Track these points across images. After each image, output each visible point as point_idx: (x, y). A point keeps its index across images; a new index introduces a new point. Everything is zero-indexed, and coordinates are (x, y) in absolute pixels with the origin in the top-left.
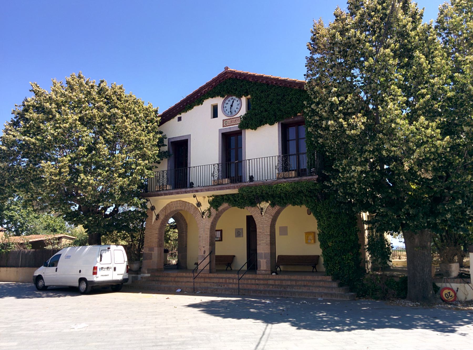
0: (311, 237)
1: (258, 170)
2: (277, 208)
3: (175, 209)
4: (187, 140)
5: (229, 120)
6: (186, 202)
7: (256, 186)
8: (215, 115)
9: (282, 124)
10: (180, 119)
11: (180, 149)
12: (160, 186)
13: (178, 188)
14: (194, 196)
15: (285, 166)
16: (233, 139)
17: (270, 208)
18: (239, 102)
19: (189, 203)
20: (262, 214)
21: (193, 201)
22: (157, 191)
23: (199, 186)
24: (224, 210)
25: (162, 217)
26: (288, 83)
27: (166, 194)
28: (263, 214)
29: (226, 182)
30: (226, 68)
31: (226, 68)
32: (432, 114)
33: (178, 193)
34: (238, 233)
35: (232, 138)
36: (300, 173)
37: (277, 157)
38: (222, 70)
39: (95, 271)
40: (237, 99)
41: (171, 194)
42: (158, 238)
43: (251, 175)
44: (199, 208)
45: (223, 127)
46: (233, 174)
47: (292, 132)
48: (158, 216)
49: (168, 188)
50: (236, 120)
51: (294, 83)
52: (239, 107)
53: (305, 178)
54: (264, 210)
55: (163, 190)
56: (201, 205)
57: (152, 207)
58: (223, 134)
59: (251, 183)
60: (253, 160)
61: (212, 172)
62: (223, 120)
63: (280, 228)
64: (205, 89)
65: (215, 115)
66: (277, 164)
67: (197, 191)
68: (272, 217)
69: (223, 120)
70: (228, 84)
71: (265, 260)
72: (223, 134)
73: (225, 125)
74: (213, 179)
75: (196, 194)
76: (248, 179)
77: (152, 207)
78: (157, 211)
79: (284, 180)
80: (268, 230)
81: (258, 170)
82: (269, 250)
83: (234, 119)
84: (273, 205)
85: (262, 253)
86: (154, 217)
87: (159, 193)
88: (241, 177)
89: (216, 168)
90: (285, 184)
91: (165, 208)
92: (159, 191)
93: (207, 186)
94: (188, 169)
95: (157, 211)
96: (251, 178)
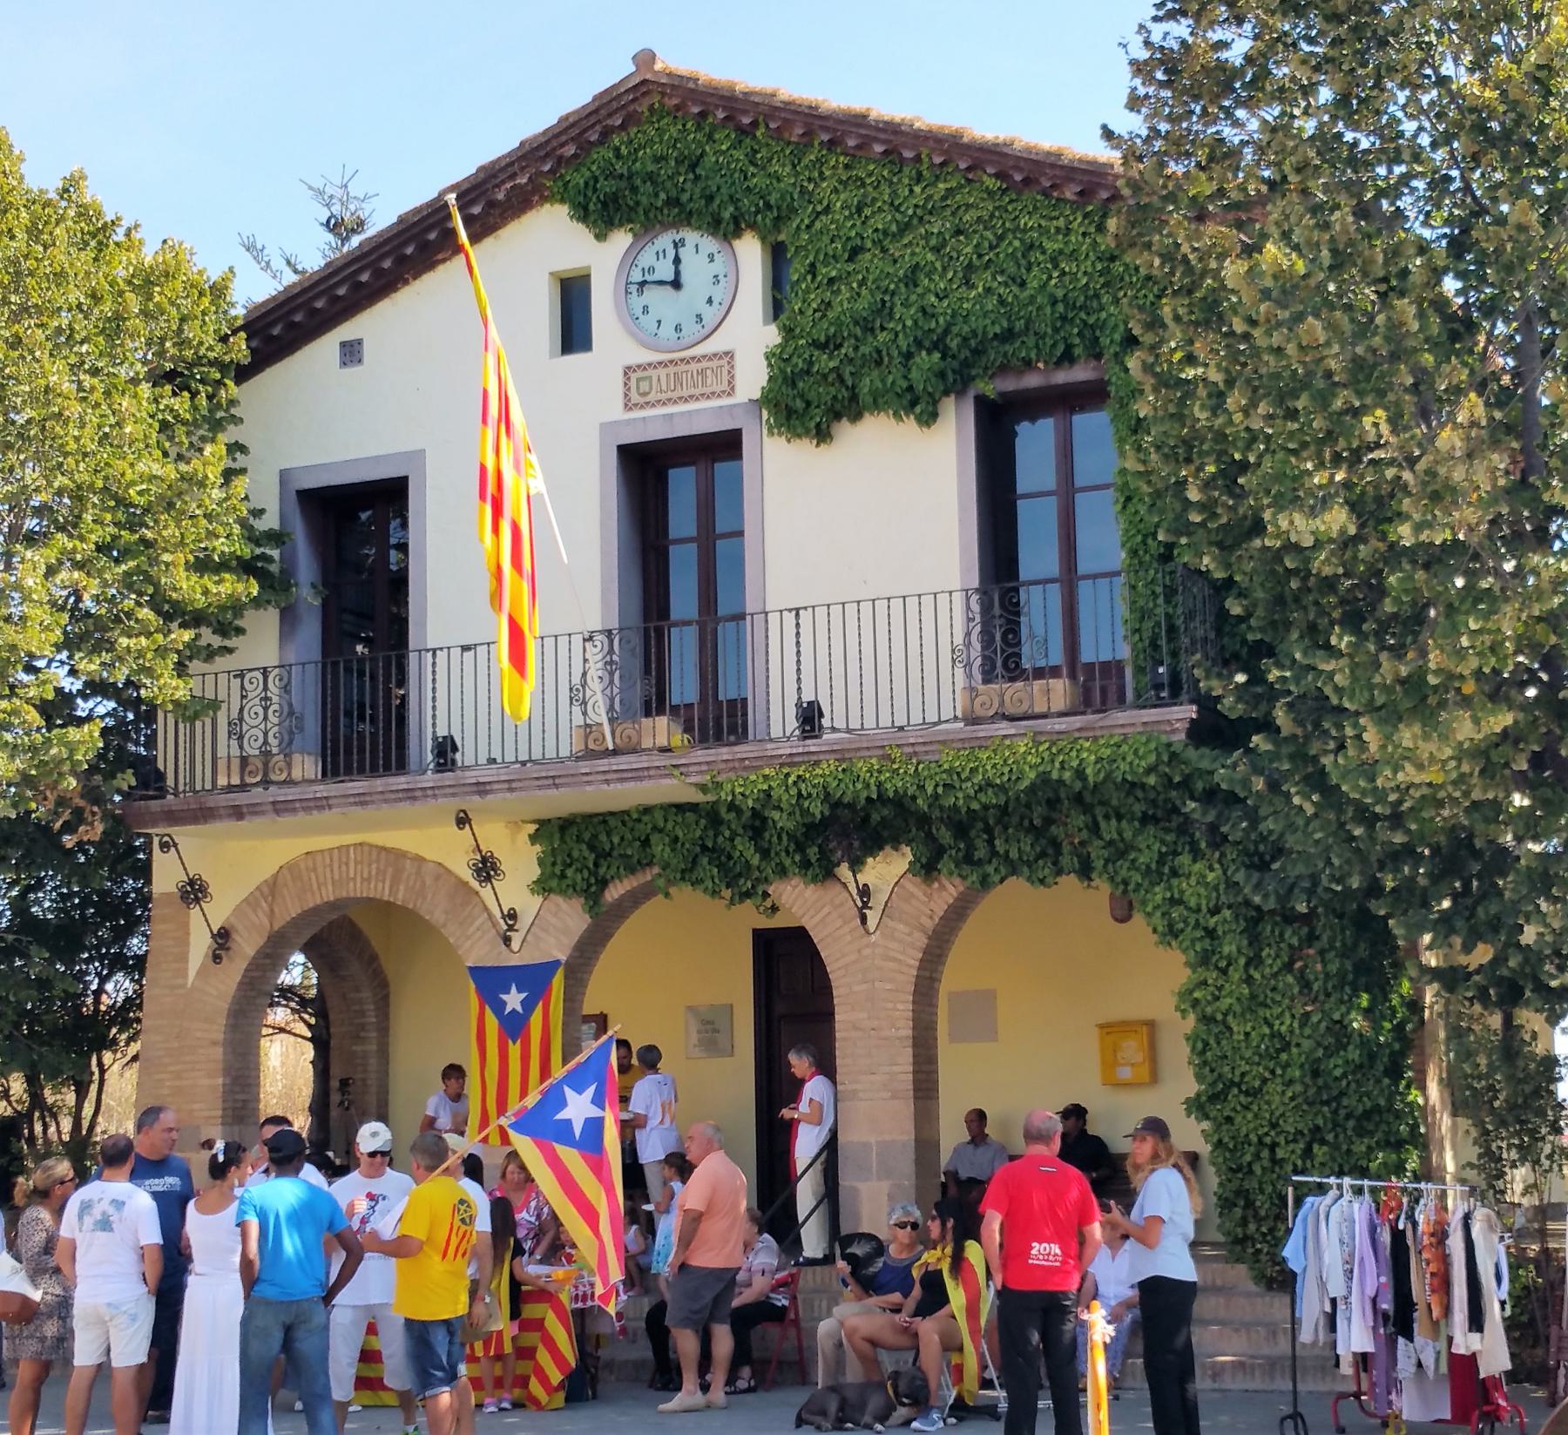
0: (1132, 1049)
1: (838, 670)
2: (949, 890)
3: (329, 894)
4: (406, 478)
5: (662, 372)
6: (400, 855)
7: (841, 754)
8: (574, 333)
9: (982, 403)
10: (351, 353)
11: (355, 536)
12: (244, 761)
13: (349, 771)
14: (463, 821)
15: (1001, 645)
16: (682, 484)
17: (914, 886)
18: (719, 266)
19: (420, 860)
20: (864, 919)
21: (450, 850)
22: (230, 789)
23: (492, 761)
24: (636, 899)
25: (247, 946)
26: (1018, 169)
27: (280, 808)
28: (872, 923)
29: (662, 741)
30: (645, 58)
31: (645, 58)
32: (643, 108)
33: (362, 800)
34: (711, 1032)
35: (673, 474)
36: (1097, 688)
37: (958, 599)
38: (614, 70)
39: (370, 1372)
40: (709, 244)
41: (322, 804)
42: (227, 1071)
43: (808, 697)
44: (486, 892)
45: (628, 406)
46: (684, 687)
47: (1035, 443)
48: (223, 938)
49: (297, 774)
50: (702, 372)
51: (1053, 166)
52: (719, 294)
53: (1120, 717)
54: (877, 901)
55: (266, 783)
56: (494, 868)
57: (191, 882)
58: (624, 450)
59: (812, 745)
60: (821, 612)
61: (576, 680)
62: (628, 371)
63: (953, 996)
64: (513, 176)
65: (574, 333)
66: (959, 639)
67: (482, 789)
68: (922, 941)
69: (628, 371)
70: (652, 157)
71: (885, 1186)
72: (624, 450)
73: (635, 398)
74: (579, 720)
75: (472, 803)
76: (792, 724)
77: (191, 882)
78: (219, 909)
79: (1004, 728)
80: (903, 1008)
81: (838, 670)
82: (910, 1126)
83: (694, 366)
84: (927, 868)
85: (867, 1146)
86: (200, 944)
87: (240, 799)
88: (738, 708)
89: (596, 653)
90: (1018, 754)
91: (272, 888)
92: (243, 787)
93: (551, 762)
94: (413, 657)
95: (219, 909)
96: (810, 717)
